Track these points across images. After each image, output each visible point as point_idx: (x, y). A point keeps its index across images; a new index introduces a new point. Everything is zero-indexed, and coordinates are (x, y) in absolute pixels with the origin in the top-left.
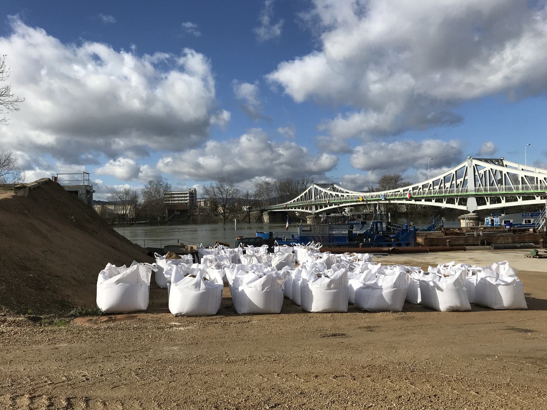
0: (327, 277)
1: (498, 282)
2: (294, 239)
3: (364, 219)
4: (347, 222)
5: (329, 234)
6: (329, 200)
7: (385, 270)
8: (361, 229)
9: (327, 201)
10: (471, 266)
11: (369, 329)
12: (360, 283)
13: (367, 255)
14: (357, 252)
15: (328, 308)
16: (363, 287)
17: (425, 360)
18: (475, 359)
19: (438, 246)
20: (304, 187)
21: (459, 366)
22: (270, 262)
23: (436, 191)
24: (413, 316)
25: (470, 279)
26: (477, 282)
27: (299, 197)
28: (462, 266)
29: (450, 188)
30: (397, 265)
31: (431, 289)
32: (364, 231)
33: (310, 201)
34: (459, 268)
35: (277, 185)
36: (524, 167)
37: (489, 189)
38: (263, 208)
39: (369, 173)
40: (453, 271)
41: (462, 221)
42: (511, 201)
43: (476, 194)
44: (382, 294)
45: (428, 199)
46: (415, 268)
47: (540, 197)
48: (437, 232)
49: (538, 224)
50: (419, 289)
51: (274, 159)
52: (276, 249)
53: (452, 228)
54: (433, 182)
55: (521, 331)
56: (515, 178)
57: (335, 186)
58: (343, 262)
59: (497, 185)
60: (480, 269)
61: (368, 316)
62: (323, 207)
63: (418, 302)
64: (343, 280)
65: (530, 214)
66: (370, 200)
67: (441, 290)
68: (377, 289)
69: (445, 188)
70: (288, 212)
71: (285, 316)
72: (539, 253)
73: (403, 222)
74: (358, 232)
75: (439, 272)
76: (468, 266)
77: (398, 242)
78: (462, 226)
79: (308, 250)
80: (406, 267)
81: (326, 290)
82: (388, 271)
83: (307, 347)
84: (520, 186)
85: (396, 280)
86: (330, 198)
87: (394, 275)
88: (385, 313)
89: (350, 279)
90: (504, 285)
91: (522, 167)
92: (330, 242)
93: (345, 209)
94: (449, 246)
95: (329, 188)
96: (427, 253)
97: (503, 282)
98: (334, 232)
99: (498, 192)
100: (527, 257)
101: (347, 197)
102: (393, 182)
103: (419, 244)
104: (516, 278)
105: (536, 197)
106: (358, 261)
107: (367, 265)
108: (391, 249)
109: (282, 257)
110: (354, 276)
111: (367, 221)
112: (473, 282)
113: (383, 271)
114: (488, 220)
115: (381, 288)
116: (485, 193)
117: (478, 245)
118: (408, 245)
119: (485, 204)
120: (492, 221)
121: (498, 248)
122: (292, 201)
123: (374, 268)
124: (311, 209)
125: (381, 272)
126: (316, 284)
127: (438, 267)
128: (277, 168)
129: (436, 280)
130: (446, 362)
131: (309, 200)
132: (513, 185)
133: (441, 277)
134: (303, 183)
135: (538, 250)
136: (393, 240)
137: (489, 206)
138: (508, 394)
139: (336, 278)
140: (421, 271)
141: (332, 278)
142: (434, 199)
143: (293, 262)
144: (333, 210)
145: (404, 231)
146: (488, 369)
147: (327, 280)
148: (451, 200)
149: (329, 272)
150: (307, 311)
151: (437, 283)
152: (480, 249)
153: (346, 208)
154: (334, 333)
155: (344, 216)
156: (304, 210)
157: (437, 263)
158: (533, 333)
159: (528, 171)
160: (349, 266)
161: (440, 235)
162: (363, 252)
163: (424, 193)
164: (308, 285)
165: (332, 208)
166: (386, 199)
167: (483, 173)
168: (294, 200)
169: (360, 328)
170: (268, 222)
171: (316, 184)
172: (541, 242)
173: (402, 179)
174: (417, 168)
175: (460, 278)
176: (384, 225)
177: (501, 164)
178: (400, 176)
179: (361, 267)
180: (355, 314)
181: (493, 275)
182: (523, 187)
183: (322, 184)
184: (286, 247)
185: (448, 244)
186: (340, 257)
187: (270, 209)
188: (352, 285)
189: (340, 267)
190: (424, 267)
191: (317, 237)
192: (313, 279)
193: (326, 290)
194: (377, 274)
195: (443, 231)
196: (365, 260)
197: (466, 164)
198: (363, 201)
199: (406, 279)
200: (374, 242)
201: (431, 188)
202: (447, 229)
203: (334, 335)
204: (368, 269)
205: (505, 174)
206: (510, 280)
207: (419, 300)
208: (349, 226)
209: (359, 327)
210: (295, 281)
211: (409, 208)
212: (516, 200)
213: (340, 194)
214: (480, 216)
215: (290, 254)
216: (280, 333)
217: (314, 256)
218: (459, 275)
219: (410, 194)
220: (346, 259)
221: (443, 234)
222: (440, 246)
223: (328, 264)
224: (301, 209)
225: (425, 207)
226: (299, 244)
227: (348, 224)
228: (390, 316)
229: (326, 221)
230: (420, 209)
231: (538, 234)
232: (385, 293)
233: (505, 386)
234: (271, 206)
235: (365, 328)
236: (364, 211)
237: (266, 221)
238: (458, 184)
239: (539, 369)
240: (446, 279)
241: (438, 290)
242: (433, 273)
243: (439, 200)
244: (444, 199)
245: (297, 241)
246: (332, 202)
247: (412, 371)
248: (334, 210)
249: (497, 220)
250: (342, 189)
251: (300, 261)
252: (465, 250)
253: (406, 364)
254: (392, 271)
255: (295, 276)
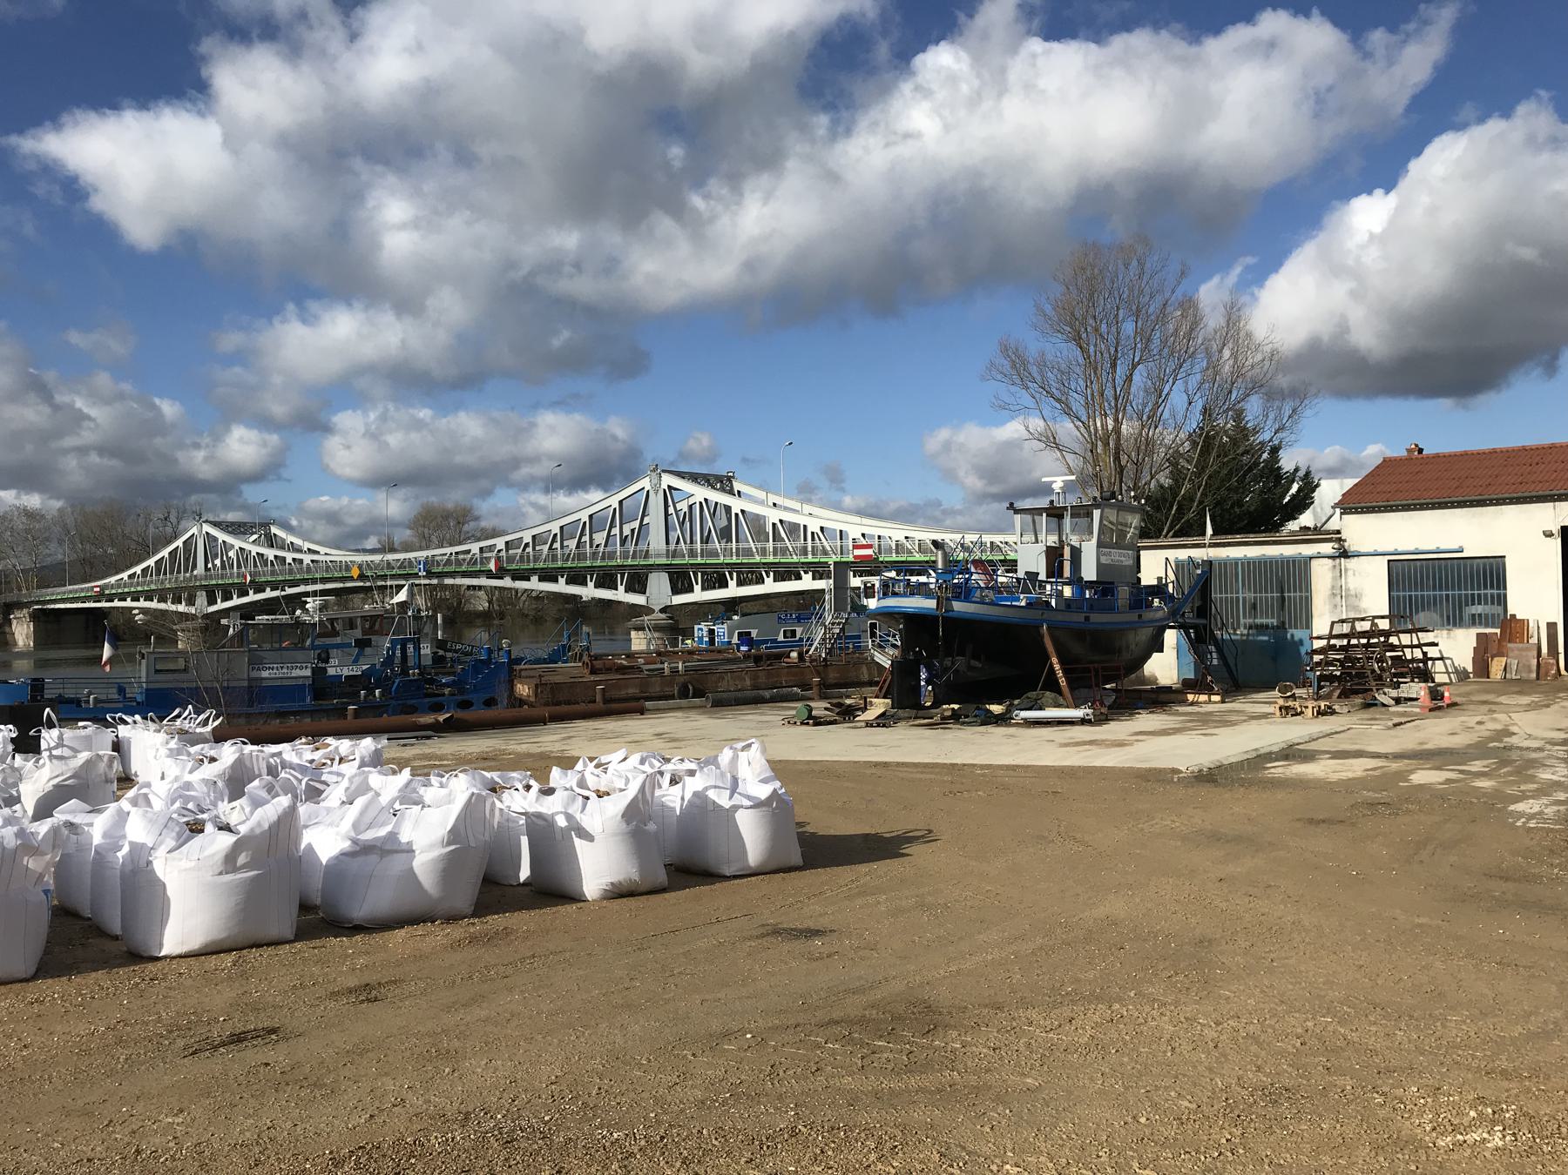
0: (226, 828)
1: (737, 800)
2: (125, 697)
3: (364, 632)
4: (308, 642)
5: (250, 679)
6: (255, 572)
7: (422, 790)
8: (356, 661)
9: (248, 576)
10: (668, 761)
11: (368, 993)
12: (339, 838)
13: (367, 744)
14: (339, 734)
15: (223, 935)
16: (349, 849)
17: (547, 1086)
18: (693, 1055)
19: (574, 704)
20: (169, 530)
21: (649, 1088)
22: (16, 785)
23: (569, 554)
24: (505, 928)
25: (664, 796)
26: (682, 805)
27: (151, 562)
28: (642, 762)
29: (606, 546)
30: (460, 772)
31: (558, 836)
32: (365, 667)
33: (188, 575)
34: (635, 768)
35: (70, 521)
36: (779, 500)
37: (699, 551)
38: (11, 597)
39: (381, 495)
40: (620, 777)
41: (633, 633)
42: (750, 583)
43: (669, 562)
44: (412, 868)
45: (549, 576)
46: (514, 774)
47: (811, 573)
48: (573, 664)
49: (809, 638)
50: (524, 841)
51: (59, 433)
52: (49, 737)
53: (611, 653)
54: (562, 528)
55: (797, 937)
56: (757, 523)
57: (274, 530)
58: (286, 773)
59: (719, 543)
60: (693, 766)
61: (365, 944)
62: (235, 597)
63: (522, 880)
64: (287, 826)
65: (794, 616)
66: (382, 576)
67: (589, 837)
68: (397, 852)
69: (591, 546)
70: (110, 612)
71: (54, 989)
72: (814, 713)
73: (480, 637)
74: (346, 672)
75: (582, 784)
76: (660, 761)
77: (460, 698)
78: (634, 648)
79: (171, 734)
80: (488, 775)
81: (221, 874)
82: (430, 793)
83: (124, 1109)
84: (770, 545)
85: (456, 821)
86: (255, 565)
87: (450, 803)
88: (420, 930)
89: (306, 827)
90: (751, 807)
91: (772, 498)
92: (253, 703)
93: (306, 603)
94: (601, 704)
95: (255, 537)
96: (545, 724)
97: (749, 797)
98: (265, 674)
99: (721, 560)
100: (789, 722)
101: (312, 565)
102: (452, 524)
103: (521, 702)
104: (777, 784)
105: (802, 573)
106: (340, 763)
107: (367, 778)
108: (441, 719)
109: (64, 768)
110: (320, 818)
111: (373, 638)
112: (672, 805)
113: (418, 793)
114: (702, 629)
115: (409, 850)
116: (690, 562)
117: (672, 697)
118: (490, 703)
119: (690, 590)
120: (711, 632)
121: (723, 703)
122: (125, 575)
123: (388, 785)
124: (191, 602)
125: (409, 797)
126: (181, 859)
127: (579, 766)
128: (71, 463)
129: (575, 809)
130: (611, 1080)
131: (186, 570)
132: (754, 542)
133: (587, 798)
134: (166, 519)
135: (812, 704)
136: (447, 691)
137: (699, 595)
138: (796, 1168)
139: (258, 831)
140: (532, 782)
141: (243, 829)
142: (562, 577)
143: (108, 781)
144: (267, 605)
145: (479, 666)
146: (732, 1084)
147: (227, 840)
148: (606, 581)
149: (233, 812)
150: (145, 955)
151: (578, 816)
152: (680, 708)
153: (309, 600)
154: (238, 1031)
155: (298, 624)
156: (169, 606)
157: (575, 753)
158: (827, 939)
159: (786, 509)
160: (307, 783)
161: (577, 673)
162: (356, 733)
163: (536, 559)
164: (149, 863)
165: (263, 600)
166: (430, 575)
167: (686, 509)
168: (131, 572)
169: (334, 995)
170: (32, 644)
171: (211, 522)
172: (814, 684)
173: (477, 519)
174: (524, 486)
175: (640, 796)
176: (426, 650)
177: (728, 488)
178: (469, 511)
179: (345, 783)
180: (321, 944)
181: (723, 782)
182: (775, 549)
183: (233, 524)
184: (88, 729)
185: (598, 698)
186: (280, 753)
187: (38, 603)
188: (314, 846)
189: (277, 788)
190: (539, 767)
191: (206, 689)
192: (171, 843)
193: (221, 874)
194: (397, 806)
195: (587, 663)
196: (361, 758)
197: (645, 483)
198: (362, 577)
199: (488, 815)
200: (392, 698)
201: (557, 545)
202: (597, 657)
203: (238, 1039)
204: (369, 789)
205: (737, 515)
206: (764, 792)
207: (525, 873)
208: (318, 652)
209: (333, 993)
210: (104, 853)
211: (494, 598)
212: (760, 581)
213: (289, 557)
214: (677, 623)
215: (98, 755)
216: (19, 1065)
217: (189, 754)
218: (637, 790)
219: (498, 559)
220: (301, 758)
221: (586, 671)
222: (579, 704)
223: (236, 783)
224: (155, 601)
225: (540, 597)
226: (137, 717)
227: (313, 647)
228: (436, 936)
229: (241, 636)
230: (525, 602)
231: (808, 664)
232: (422, 864)
233: (786, 1136)
234: (44, 591)
235: (351, 992)
236: (366, 606)
237: (21, 643)
238: (624, 535)
239: (863, 1058)
240: (602, 803)
241: (580, 837)
242: (566, 789)
243: (577, 578)
244: (589, 576)
245: (135, 704)
246: (263, 579)
247: (507, 1142)
248: (272, 605)
249: (721, 629)
250: (298, 541)
251: (138, 773)
252: (642, 711)
253: (486, 1113)
254: (444, 791)
255: (105, 835)
